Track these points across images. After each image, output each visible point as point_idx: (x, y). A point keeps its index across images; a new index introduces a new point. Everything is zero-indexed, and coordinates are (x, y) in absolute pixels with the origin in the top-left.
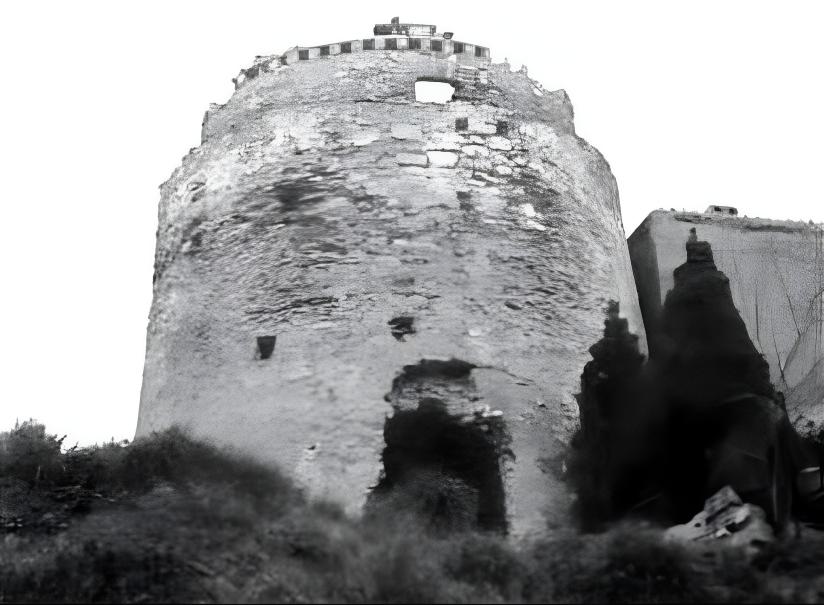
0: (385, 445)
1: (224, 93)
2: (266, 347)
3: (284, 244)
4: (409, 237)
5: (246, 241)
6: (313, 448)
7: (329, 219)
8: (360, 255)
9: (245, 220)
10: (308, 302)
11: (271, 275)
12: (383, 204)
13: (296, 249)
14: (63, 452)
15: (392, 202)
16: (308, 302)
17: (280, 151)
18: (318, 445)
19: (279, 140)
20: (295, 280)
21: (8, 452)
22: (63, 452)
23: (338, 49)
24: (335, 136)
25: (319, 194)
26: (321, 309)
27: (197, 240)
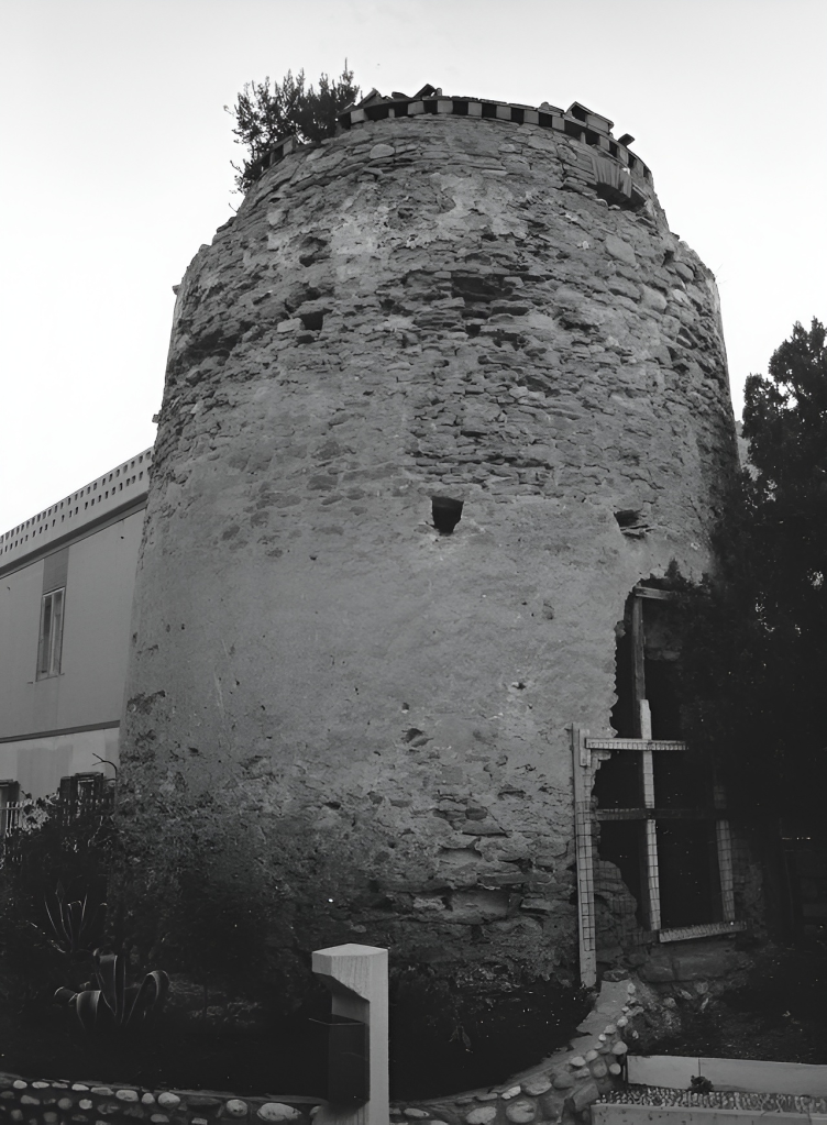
0: (615, 699)
1: (244, 153)
2: (446, 516)
3: (473, 364)
4: (629, 393)
5: (404, 343)
6: (521, 687)
8: (572, 402)
9: (400, 311)
10: (511, 460)
11: (451, 403)
12: (601, 340)
13: (487, 375)
14: (697, 579)
15: (612, 341)
16: (511, 460)
17: (460, 224)
18: (529, 684)
19: (459, 210)
20: (706, 386)
21: (640, 548)
22: (697, 579)
23: (507, 114)
24: (536, 226)
25: (519, 304)
26: (532, 472)
27: (313, 321)
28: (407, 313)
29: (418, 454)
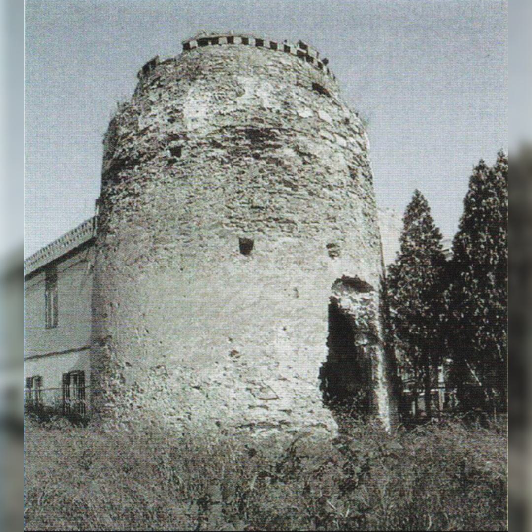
7: (286, 163)
28: (224, 147)
29: (230, 218)
